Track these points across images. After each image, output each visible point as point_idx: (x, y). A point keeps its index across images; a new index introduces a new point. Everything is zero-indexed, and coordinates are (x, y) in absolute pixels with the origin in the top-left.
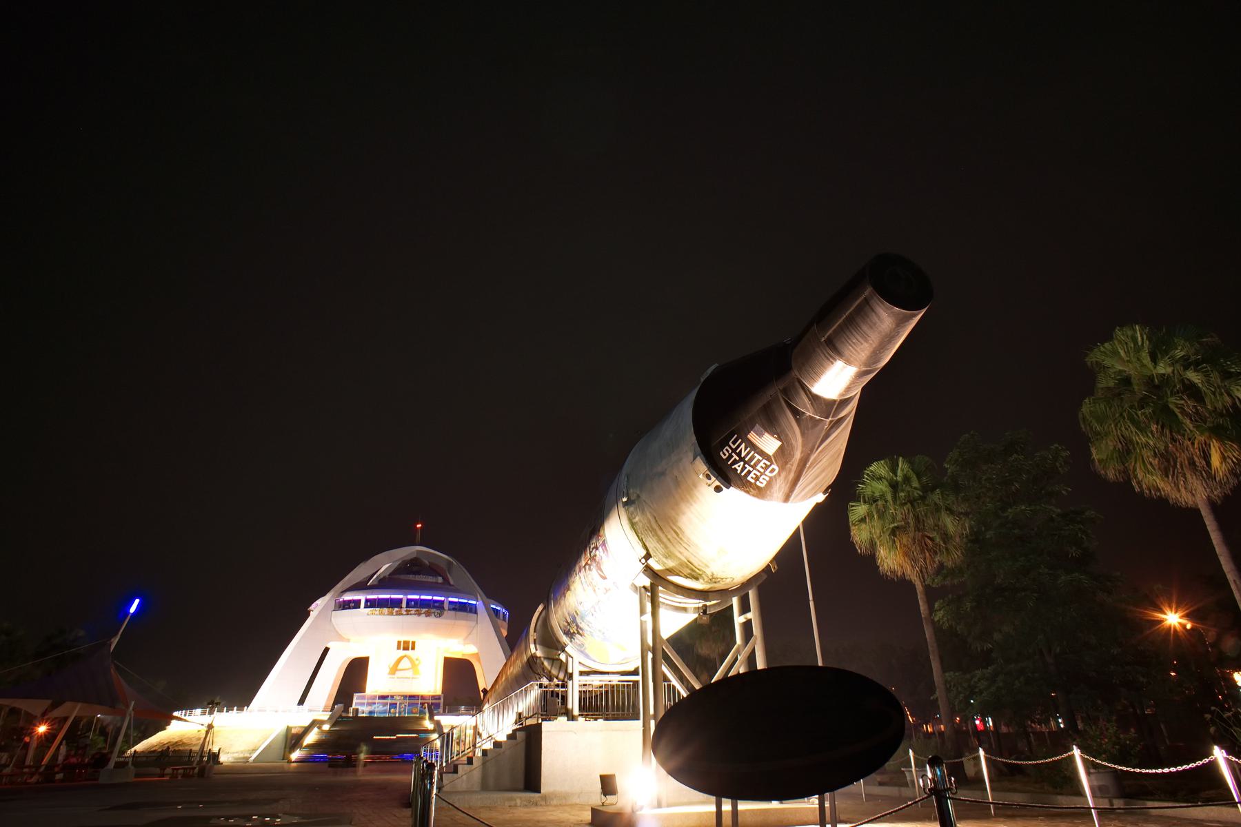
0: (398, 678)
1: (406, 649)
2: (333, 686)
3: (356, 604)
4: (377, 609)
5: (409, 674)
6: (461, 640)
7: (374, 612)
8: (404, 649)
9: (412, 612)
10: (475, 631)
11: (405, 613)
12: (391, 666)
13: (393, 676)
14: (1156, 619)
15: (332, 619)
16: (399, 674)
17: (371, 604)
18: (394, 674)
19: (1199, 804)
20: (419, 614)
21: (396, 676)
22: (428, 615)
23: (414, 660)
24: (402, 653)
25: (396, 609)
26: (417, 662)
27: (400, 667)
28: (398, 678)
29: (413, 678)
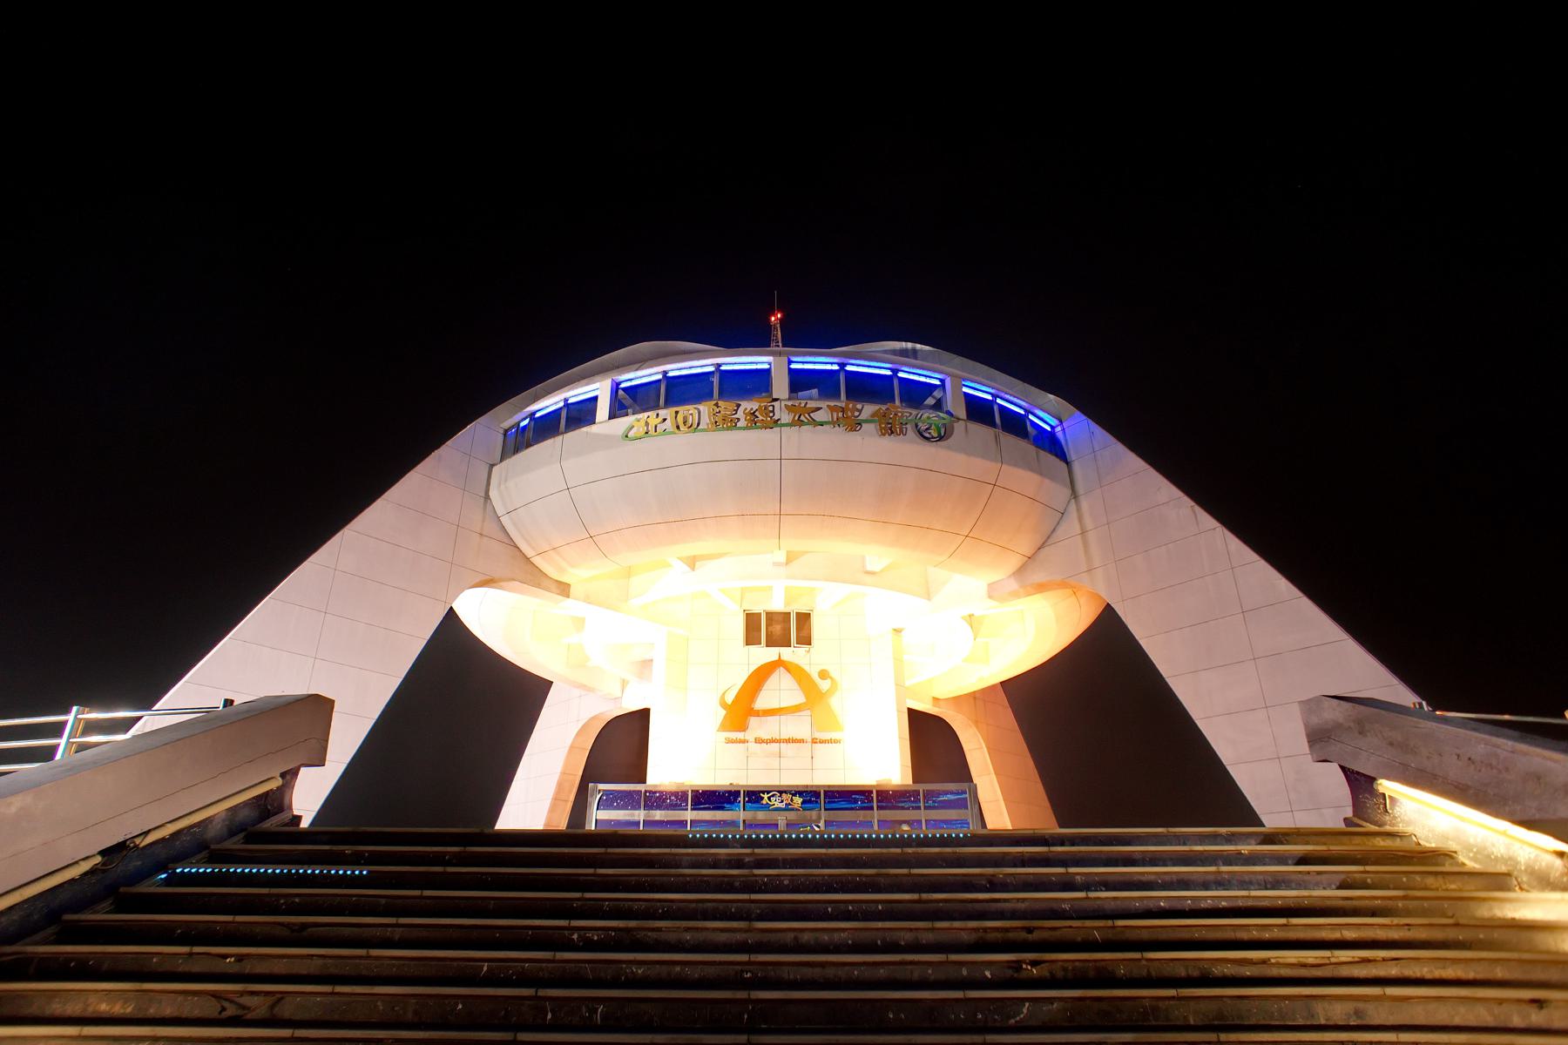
0: (759, 741)
1: (782, 641)
2: (556, 799)
3: (581, 414)
4: (663, 413)
5: (796, 727)
6: (999, 571)
7: (653, 421)
8: (771, 643)
9: (818, 416)
10: (1071, 526)
11: (786, 418)
12: (730, 699)
13: (740, 735)
14: (1397, 844)
15: (493, 493)
16: (758, 728)
17: (628, 401)
18: (743, 728)
19: (354, 899)
20: (855, 425)
21: (750, 735)
22: (890, 428)
23: (815, 676)
24: (764, 654)
25: (748, 405)
26: (824, 685)
27: (762, 702)
28: (759, 741)
29: (814, 741)
